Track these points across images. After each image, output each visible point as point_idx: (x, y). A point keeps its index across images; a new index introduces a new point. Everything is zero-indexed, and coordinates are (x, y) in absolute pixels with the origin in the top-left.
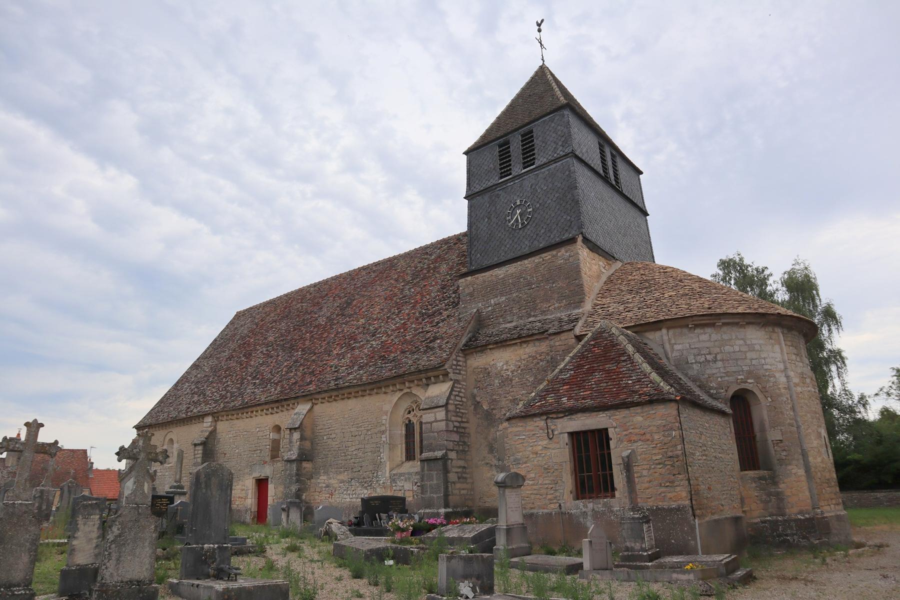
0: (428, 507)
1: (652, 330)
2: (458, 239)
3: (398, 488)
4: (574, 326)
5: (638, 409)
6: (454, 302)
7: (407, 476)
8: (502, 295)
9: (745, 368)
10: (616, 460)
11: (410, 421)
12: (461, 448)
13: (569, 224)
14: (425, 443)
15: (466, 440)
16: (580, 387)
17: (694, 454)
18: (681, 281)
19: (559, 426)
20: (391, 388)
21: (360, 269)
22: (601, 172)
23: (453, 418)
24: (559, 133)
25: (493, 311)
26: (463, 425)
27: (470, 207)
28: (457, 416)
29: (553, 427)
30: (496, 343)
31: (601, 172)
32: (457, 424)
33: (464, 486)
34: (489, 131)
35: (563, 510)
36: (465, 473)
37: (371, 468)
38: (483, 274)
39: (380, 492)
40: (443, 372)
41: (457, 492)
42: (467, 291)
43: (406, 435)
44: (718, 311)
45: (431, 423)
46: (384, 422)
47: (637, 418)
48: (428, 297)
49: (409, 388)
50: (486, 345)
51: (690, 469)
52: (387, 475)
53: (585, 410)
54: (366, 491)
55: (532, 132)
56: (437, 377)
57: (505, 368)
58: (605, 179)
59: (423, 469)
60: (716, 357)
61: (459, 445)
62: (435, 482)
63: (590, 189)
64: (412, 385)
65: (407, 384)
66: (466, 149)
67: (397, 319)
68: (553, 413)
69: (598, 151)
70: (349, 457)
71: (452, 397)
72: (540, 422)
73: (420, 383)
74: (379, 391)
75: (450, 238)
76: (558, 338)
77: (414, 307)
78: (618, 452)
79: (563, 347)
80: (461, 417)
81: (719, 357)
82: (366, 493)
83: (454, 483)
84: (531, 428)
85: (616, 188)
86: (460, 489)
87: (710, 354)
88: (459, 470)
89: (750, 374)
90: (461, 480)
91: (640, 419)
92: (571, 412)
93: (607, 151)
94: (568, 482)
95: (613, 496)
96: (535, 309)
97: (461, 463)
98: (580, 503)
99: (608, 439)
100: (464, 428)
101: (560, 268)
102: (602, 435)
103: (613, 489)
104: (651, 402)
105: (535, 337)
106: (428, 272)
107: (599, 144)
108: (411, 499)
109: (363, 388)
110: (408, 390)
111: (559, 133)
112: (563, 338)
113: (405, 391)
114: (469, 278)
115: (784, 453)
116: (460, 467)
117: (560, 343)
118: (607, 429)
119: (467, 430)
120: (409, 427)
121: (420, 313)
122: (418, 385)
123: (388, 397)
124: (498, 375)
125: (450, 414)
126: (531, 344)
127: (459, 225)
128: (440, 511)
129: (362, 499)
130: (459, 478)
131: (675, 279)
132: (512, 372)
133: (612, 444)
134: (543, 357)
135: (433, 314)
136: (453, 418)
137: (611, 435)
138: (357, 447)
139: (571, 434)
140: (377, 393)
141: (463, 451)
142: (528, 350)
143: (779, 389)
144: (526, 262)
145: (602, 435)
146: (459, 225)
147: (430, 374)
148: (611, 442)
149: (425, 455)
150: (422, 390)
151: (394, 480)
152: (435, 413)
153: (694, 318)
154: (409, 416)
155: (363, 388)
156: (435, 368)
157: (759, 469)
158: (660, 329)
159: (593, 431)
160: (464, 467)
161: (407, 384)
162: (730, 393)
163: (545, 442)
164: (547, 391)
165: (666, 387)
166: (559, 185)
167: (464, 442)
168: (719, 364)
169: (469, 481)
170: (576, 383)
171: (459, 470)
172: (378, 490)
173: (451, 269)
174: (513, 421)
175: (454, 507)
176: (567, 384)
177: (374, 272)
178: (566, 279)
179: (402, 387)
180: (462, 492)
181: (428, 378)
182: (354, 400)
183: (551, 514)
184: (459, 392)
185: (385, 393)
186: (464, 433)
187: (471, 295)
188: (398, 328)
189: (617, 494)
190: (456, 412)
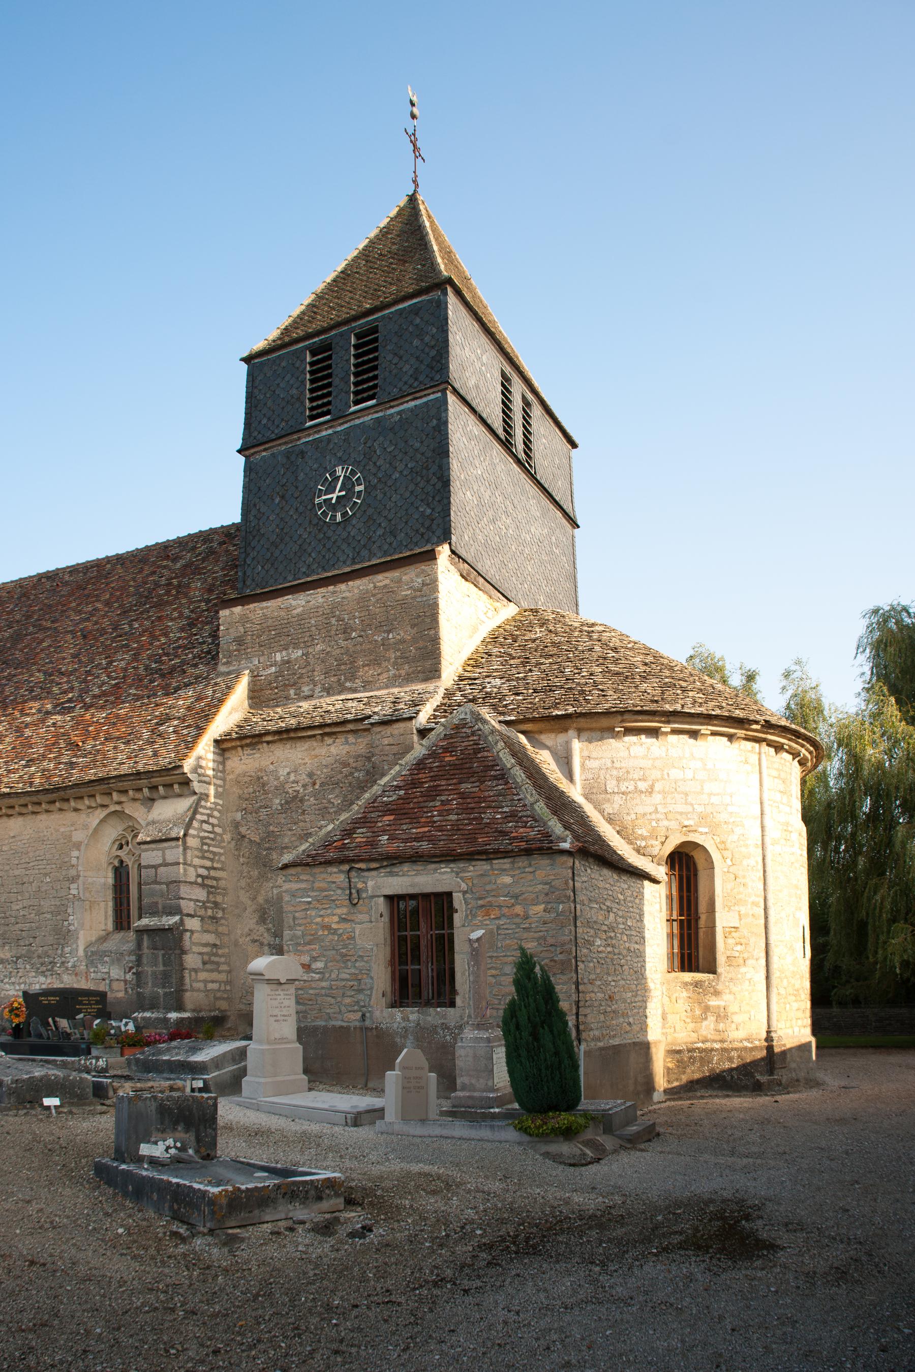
0: (152, 1007)
1: (552, 731)
2: (227, 533)
3: (99, 976)
4: (417, 713)
5: (505, 863)
6: (209, 652)
7: (118, 958)
8: (296, 646)
9: (699, 809)
10: (460, 946)
11: (121, 862)
12: (210, 912)
13: (427, 523)
14: (145, 901)
15: (219, 899)
16: (414, 820)
17: (592, 943)
18: (615, 649)
19: (370, 884)
20: (87, 802)
21: (40, 577)
22: (500, 432)
23: (197, 861)
24: (427, 339)
25: (279, 674)
26: (213, 873)
27: (249, 470)
28: (203, 858)
29: (360, 885)
30: (279, 732)
31: (500, 432)
32: (202, 872)
33: (215, 976)
34: (298, 322)
35: (368, 1023)
36: (216, 955)
37: (50, 940)
38: (264, 604)
39: (68, 981)
40: (180, 779)
41: (197, 985)
42: (233, 634)
43: (115, 886)
44: (668, 707)
45: (156, 867)
46: (74, 861)
47: (504, 876)
48: (163, 640)
49: (120, 803)
50: (260, 735)
51: (581, 966)
52: (81, 952)
53: (416, 858)
54: (42, 979)
55: (375, 330)
56: (169, 786)
57: (292, 777)
58: (507, 445)
59: (139, 945)
60: (652, 787)
61: (206, 908)
62: (161, 968)
63: (473, 460)
64: (123, 799)
65: (115, 796)
66: (245, 354)
67: (104, 678)
68: (362, 861)
69: (500, 388)
70: (13, 920)
71: (195, 824)
72: (337, 876)
73: (138, 795)
74: (65, 806)
75: (213, 531)
76: (388, 730)
77: (135, 657)
78: (468, 932)
79: (395, 749)
80: (212, 860)
81: (657, 787)
82: (39, 983)
83: (196, 971)
84: (323, 885)
85: (525, 464)
86: (205, 982)
87: (644, 779)
88: (205, 950)
89: (702, 817)
90: (208, 966)
91: (508, 880)
92: (393, 860)
93: (518, 389)
94: (380, 977)
95: (452, 1004)
96: (353, 678)
97: (210, 938)
98: (398, 1013)
99: (452, 910)
100: (216, 879)
101: (404, 604)
102: (442, 903)
103: (453, 992)
104: (528, 852)
105: (350, 727)
106: (168, 593)
107: (503, 375)
108: (121, 995)
109: (34, 799)
110: (118, 808)
111: (427, 339)
112: (396, 732)
113: (113, 808)
114: (238, 610)
115: (739, 948)
116: (206, 945)
117: (391, 740)
118: (449, 895)
119: (222, 883)
120: (120, 872)
121: (147, 668)
122: (134, 800)
123: (81, 818)
124: (280, 788)
125: (189, 853)
126: (341, 739)
127: (226, 510)
128: (170, 1015)
129: (26, 994)
130: (204, 963)
131: (605, 645)
132: (304, 786)
133: (457, 919)
134: (359, 764)
135: (173, 670)
136: (197, 861)
137: (456, 904)
138: (26, 903)
139: (391, 899)
140: (61, 810)
141: (213, 918)
142: (336, 749)
143: (746, 846)
144: (343, 587)
145: (442, 903)
146: (226, 510)
147: (156, 780)
148: (456, 916)
149: (145, 921)
150: (143, 810)
151: (92, 962)
152: (163, 850)
153: (626, 717)
154: (119, 853)
155: (34, 799)
156: (165, 771)
157: (698, 970)
158: (566, 730)
159: (426, 896)
160: (215, 945)
161: (115, 796)
162: (669, 848)
163: (345, 910)
164: (358, 823)
165: (556, 827)
166: (417, 445)
167: (216, 904)
168: (657, 798)
169: (224, 967)
170: (402, 810)
171: (205, 950)
172: (65, 977)
173: (210, 591)
174: (292, 871)
175: (194, 1011)
176: (390, 812)
177: (66, 583)
178: (413, 626)
179: (105, 800)
180: (210, 986)
181: (154, 788)
182: (20, 820)
183: (348, 1028)
184: (209, 815)
185: (76, 810)
186: (216, 888)
187: (240, 641)
188: (104, 694)
189: (459, 1000)
190: (201, 850)
